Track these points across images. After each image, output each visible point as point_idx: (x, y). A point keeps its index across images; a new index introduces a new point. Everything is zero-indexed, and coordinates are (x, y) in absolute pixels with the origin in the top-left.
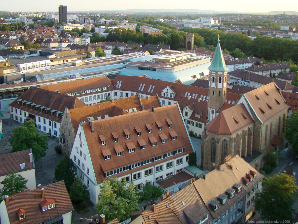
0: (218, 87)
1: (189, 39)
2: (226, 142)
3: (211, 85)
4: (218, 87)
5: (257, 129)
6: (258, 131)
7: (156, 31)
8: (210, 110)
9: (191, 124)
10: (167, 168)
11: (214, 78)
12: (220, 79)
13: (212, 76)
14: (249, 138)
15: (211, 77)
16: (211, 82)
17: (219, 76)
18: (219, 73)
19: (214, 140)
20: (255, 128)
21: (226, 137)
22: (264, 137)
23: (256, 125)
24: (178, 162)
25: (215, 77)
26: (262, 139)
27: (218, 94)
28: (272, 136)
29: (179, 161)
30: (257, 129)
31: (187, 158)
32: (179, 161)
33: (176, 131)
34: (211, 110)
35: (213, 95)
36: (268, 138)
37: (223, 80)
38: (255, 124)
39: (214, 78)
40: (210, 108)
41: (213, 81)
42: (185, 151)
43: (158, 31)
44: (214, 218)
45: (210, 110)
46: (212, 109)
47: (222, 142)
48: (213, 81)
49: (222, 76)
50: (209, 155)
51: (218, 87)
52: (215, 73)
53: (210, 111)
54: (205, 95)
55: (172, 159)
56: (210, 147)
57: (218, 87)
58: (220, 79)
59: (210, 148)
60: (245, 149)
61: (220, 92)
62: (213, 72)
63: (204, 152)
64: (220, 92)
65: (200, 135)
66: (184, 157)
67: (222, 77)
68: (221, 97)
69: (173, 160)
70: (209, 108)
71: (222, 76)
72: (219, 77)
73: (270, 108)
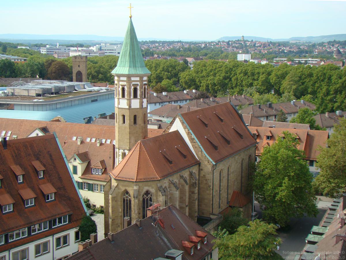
0: (133, 107)
1: (79, 66)
2: (149, 196)
3: (119, 103)
4: (133, 107)
5: (204, 176)
6: (206, 180)
7: (15, 60)
8: (120, 153)
9: (85, 188)
10: (36, 255)
11: (123, 89)
12: (135, 90)
13: (121, 87)
14: (192, 192)
15: (119, 87)
16: (119, 99)
17: (133, 85)
18: (133, 79)
19: (127, 195)
20: (202, 175)
21: (149, 186)
22: (217, 191)
23: (202, 170)
24: (58, 244)
25: (126, 88)
26: (214, 194)
27: (132, 120)
28: (231, 192)
29: (62, 240)
30: (204, 176)
31: (77, 234)
32: (62, 240)
33: (53, 184)
34: (121, 154)
35: (124, 122)
36: (224, 195)
37: (141, 92)
38: (201, 168)
39: (123, 89)
40: (119, 149)
41: (123, 96)
42: (73, 221)
43: (19, 61)
44: (123, 117)
45: (119, 152)
46: (123, 151)
47: (143, 196)
48: (123, 96)
49: (139, 84)
50: (119, 226)
51: (132, 107)
52: (125, 79)
53: (119, 155)
54: (109, 139)
55: (47, 236)
56: (120, 210)
57: (132, 107)
58: (135, 90)
59: (121, 212)
60: (186, 211)
61: (135, 117)
62: (122, 78)
63: (110, 221)
64: (135, 117)
65: (102, 207)
66: (72, 233)
67: (138, 88)
68: (137, 126)
69: (50, 238)
70: (117, 149)
71: (139, 84)
72: (133, 87)
73: (228, 142)
